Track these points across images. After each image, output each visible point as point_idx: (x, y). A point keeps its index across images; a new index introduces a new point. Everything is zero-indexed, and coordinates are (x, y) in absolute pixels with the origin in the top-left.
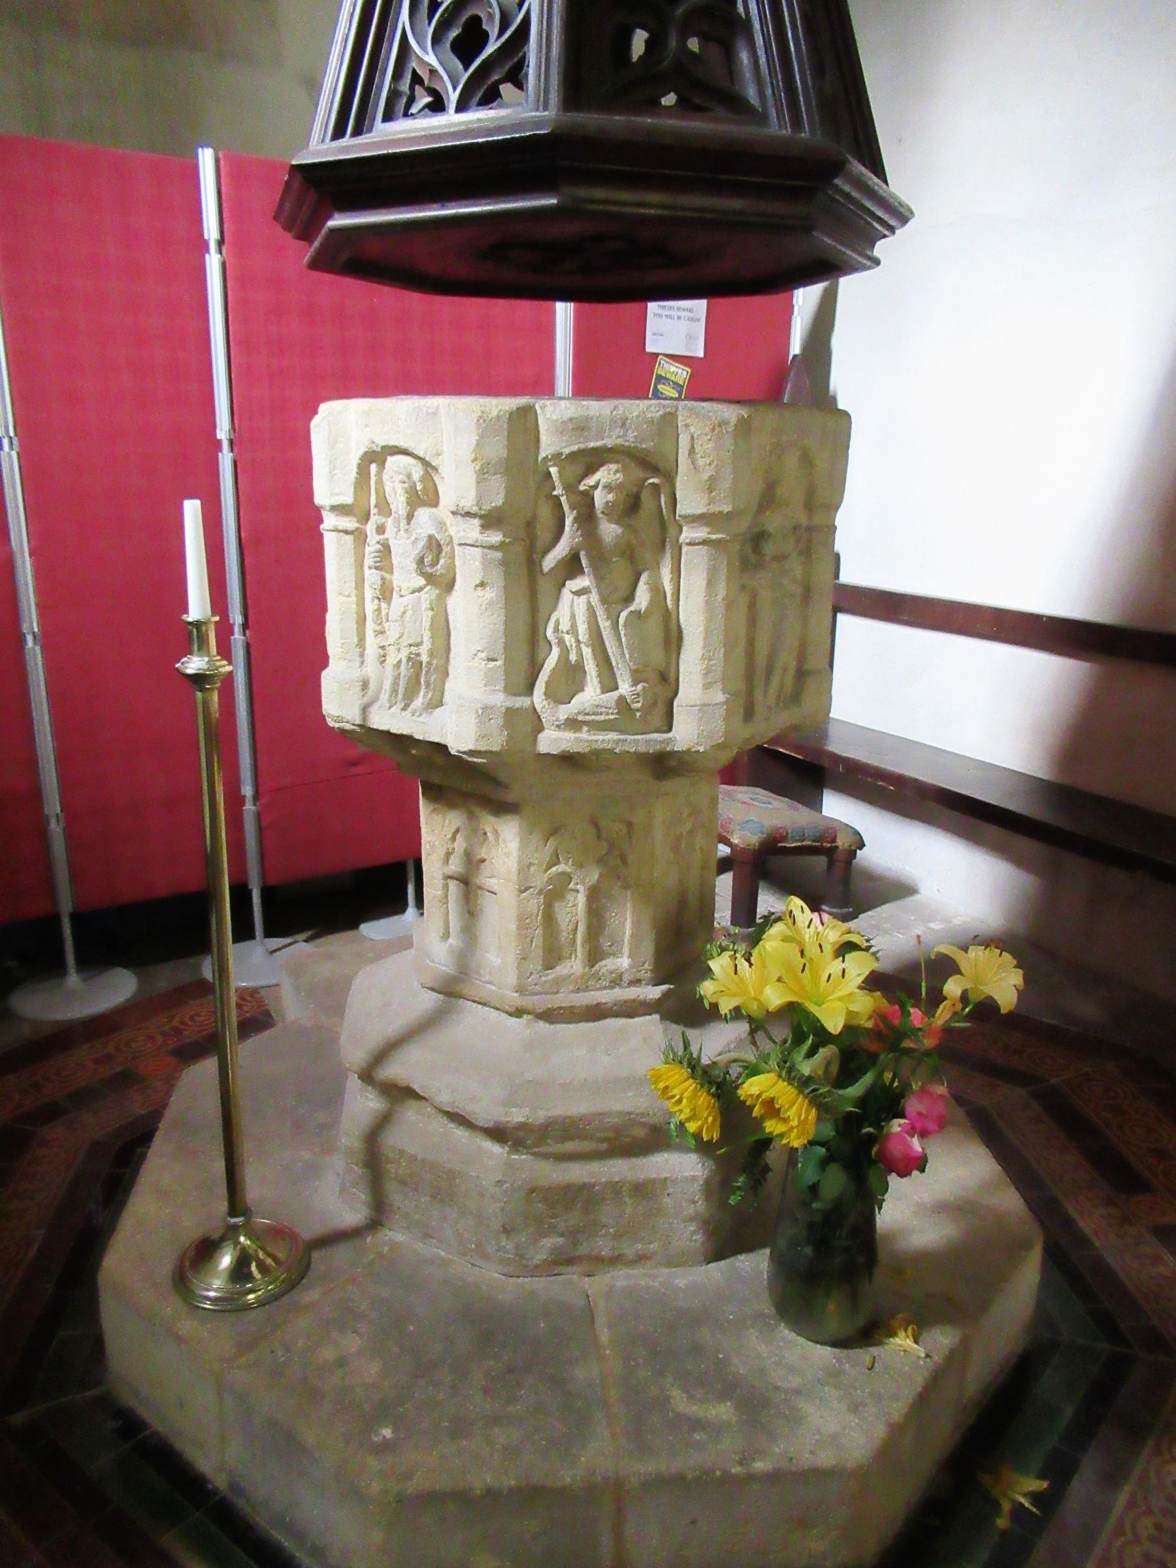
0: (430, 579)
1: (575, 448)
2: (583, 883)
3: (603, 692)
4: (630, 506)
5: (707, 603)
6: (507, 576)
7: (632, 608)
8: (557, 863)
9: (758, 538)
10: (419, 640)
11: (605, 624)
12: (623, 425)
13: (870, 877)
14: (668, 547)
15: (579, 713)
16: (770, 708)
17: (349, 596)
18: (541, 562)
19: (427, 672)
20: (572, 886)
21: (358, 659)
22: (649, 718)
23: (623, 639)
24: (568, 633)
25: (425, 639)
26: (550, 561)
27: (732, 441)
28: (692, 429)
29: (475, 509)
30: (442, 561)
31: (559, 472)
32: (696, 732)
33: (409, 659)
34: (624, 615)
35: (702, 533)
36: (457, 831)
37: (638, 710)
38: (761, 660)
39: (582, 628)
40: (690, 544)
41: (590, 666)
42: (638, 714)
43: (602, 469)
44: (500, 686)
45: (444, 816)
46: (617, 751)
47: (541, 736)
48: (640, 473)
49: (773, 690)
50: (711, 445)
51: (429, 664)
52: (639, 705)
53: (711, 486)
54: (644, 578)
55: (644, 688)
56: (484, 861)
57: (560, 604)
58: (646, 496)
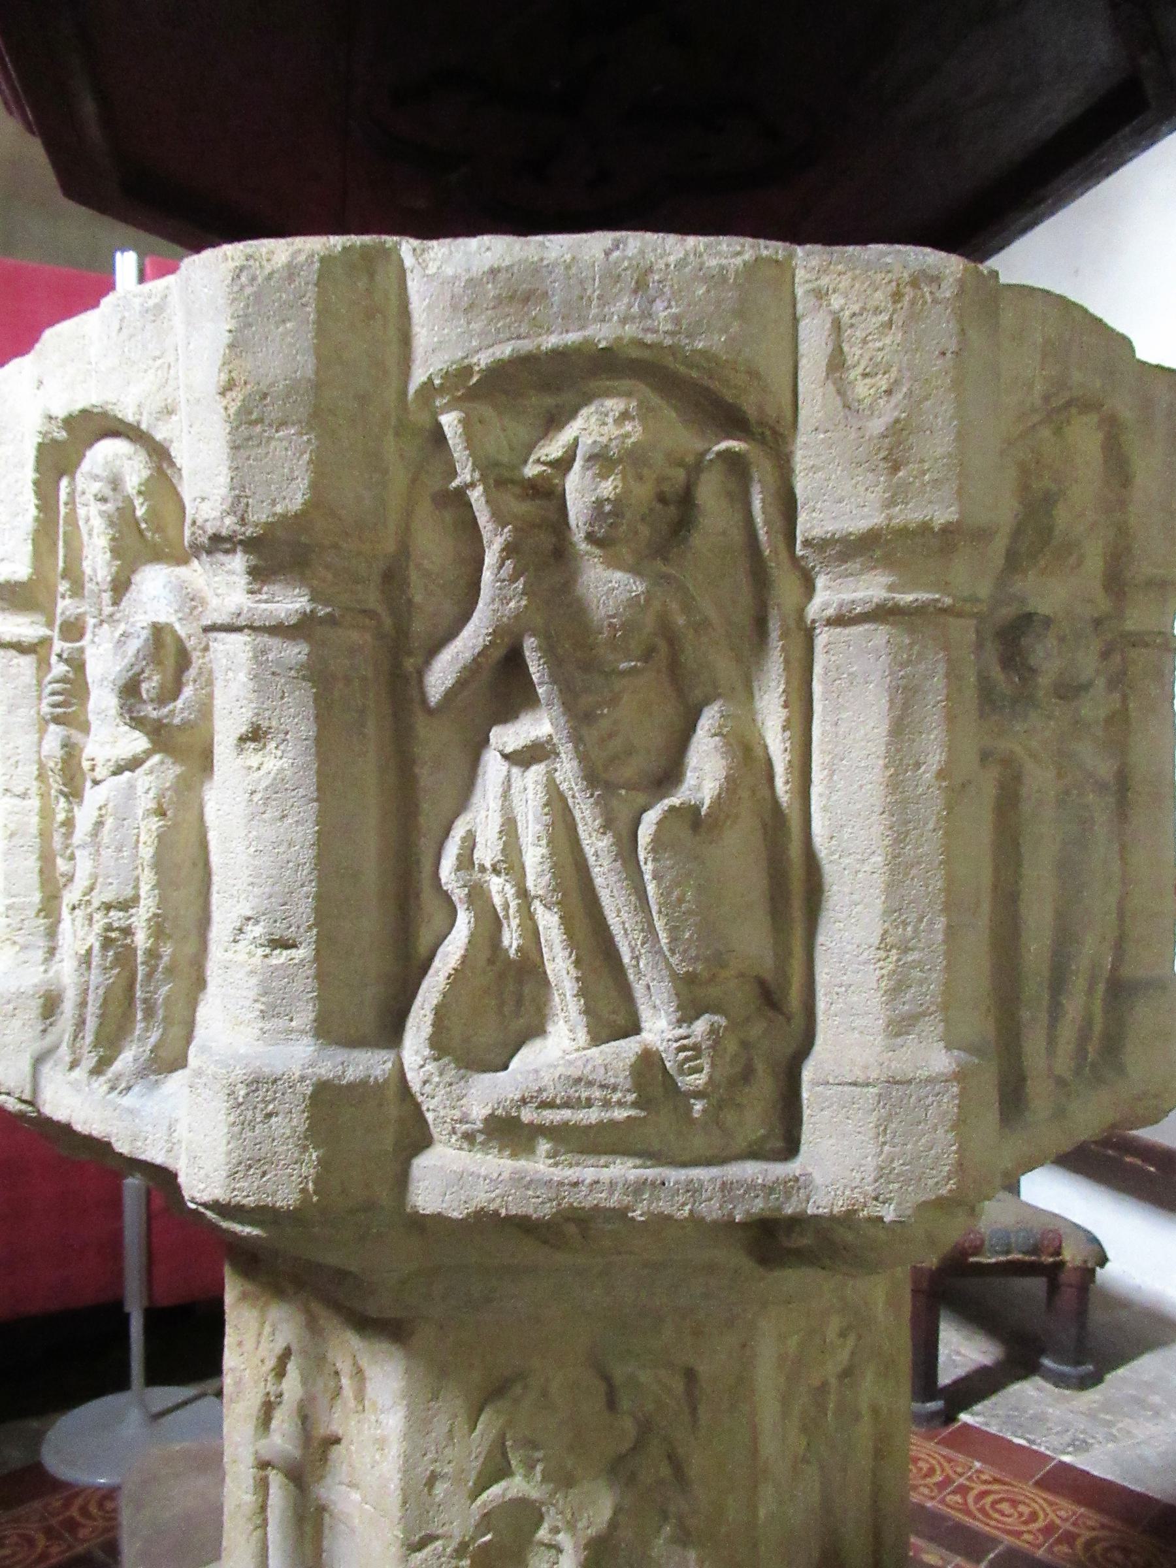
0: (162, 736)
1: (505, 351)
2: (571, 1526)
3: (597, 1039)
4: (664, 523)
5: (894, 785)
6: (325, 712)
7: (674, 801)
8: (501, 1471)
9: (1013, 637)
10: (129, 892)
11: (597, 846)
12: (640, 286)
13: (1119, 1303)
14: (774, 634)
15: (524, 1101)
16: (1061, 1082)
17: (24, 796)
18: (420, 674)
19: (149, 976)
20: (543, 1534)
21: (42, 943)
22: (730, 1117)
23: (651, 888)
24: (496, 871)
25: (144, 889)
26: (441, 674)
27: (953, 326)
28: (836, 302)
29: (229, 524)
30: (188, 692)
31: (466, 423)
32: (871, 1163)
33: (107, 943)
34: (650, 819)
35: (870, 588)
36: (286, 1355)
37: (699, 1094)
38: (1036, 948)
39: (534, 856)
40: (840, 620)
41: (559, 966)
42: (698, 1106)
43: (584, 412)
44: (305, 1017)
45: (263, 1311)
46: (637, 1215)
47: (422, 1164)
48: (683, 438)
49: (1067, 1033)
50: (893, 337)
51: (153, 954)
52: (698, 1080)
53: (894, 451)
54: (709, 719)
55: (713, 1030)
56: (337, 1441)
57: (477, 798)
58: (710, 493)
